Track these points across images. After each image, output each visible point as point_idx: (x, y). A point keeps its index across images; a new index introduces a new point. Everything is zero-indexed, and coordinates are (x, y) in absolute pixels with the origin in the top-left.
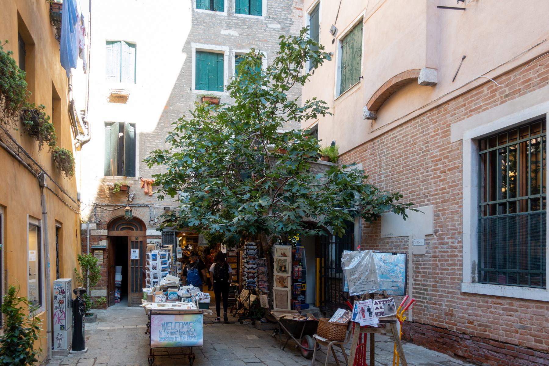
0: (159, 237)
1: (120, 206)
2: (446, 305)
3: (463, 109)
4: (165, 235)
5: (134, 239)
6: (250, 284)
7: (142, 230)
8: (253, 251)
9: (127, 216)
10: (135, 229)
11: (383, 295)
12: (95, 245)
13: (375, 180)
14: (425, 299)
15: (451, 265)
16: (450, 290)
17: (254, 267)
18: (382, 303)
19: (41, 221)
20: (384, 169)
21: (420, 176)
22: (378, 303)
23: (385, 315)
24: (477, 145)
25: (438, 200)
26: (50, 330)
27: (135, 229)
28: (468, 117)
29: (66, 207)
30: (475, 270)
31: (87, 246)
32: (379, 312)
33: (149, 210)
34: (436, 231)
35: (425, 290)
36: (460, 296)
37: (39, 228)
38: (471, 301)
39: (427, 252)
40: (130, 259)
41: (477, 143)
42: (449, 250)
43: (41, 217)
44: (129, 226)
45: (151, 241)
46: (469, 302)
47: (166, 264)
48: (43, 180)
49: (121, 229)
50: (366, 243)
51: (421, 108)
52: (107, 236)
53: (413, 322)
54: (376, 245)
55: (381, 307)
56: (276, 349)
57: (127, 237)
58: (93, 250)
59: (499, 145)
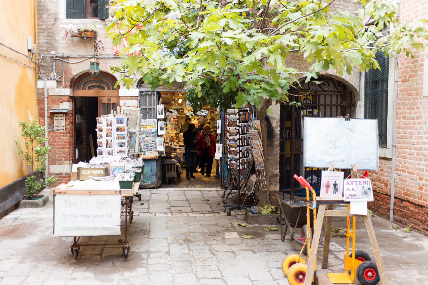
1: (88, 57)
4: (143, 96)
5: (105, 100)
6: (232, 162)
9: (93, 70)
10: (106, 88)
11: (158, 136)
12: (56, 108)
13: (417, 11)
17: (236, 139)
18: (354, 183)
22: (350, 183)
23: (357, 198)
27: (106, 88)
31: (44, 109)
32: (350, 195)
40: (303, 166)
44: (98, 84)
45: (125, 104)
49: (89, 87)
50: (403, 104)
52: (69, 96)
54: (415, 107)
55: (353, 189)
56: (257, 255)
57: (96, 98)
58: (52, 114)
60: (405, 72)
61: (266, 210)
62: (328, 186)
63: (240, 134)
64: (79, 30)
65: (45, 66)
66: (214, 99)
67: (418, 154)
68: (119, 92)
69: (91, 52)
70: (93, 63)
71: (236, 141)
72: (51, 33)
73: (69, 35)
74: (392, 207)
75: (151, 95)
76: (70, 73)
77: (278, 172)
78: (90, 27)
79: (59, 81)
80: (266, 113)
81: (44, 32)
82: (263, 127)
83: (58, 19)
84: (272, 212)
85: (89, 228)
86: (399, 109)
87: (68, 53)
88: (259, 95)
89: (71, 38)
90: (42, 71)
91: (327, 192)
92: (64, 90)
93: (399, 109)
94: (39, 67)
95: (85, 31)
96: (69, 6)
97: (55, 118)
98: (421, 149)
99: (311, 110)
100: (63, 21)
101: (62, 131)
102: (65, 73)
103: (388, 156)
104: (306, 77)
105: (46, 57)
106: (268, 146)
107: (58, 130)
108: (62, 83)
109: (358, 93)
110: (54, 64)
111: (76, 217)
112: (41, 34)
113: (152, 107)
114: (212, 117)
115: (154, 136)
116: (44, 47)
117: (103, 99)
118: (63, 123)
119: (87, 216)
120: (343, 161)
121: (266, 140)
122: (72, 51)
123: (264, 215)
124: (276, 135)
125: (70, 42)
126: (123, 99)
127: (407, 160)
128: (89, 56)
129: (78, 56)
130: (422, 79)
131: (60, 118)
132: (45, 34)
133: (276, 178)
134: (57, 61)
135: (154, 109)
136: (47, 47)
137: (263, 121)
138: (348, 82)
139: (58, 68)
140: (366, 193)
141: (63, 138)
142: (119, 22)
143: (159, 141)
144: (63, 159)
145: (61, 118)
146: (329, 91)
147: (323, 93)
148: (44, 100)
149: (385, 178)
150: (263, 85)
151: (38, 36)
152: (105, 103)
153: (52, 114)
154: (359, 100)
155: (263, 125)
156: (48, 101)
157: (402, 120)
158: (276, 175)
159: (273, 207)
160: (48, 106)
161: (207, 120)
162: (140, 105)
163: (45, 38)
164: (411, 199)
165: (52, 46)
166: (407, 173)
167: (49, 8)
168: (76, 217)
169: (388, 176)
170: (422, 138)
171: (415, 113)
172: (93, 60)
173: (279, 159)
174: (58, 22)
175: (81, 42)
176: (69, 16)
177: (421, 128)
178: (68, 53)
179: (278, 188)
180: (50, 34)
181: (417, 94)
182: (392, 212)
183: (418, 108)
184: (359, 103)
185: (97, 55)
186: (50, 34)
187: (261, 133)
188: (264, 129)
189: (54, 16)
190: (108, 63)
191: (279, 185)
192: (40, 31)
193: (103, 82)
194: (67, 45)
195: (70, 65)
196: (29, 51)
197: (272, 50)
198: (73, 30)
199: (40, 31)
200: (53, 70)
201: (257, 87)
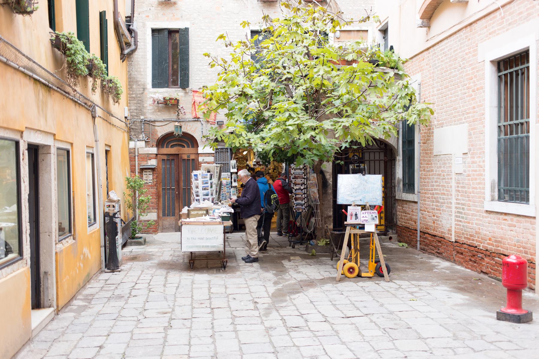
0: (213, 155)
2: (476, 224)
3: (485, 30)
4: (219, 152)
5: (185, 157)
7: (194, 147)
8: (299, 171)
13: (430, 92)
14: (463, 218)
15: (479, 184)
16: (479, 209)
18: (367, 213)
19: (95, 148)
20: (436, 82)
21: (460, 92)
24: (497, 66)
25: (471, 119)
26: (103, 244)
27: (186, 146)
28: (488, 39)
29: (114, 129)
30: (494, 188)
31: (135, 166)
33: (200, 125)
34: (470, 150)
35: (463, 209)
36: (485, 214)
37: (93, 155)
38: (491, 218)
39: (465, 171)
41: (496, 64)
42: (478, 169)
43: (94, 145)
44: (179, 143)
46: (489, 219)
47: (207, 183)
48: (95, 112)
49: (171, 146)
51: (459, 24)
53: (456, 242)
54: (430, 162)
56: (313, 266)
58: (142, 170)
59: (521, 65)
60: (424, 136)
61: (322, 243)
62: (352, 215)
63: (305, 185)
64: (164, 98)
65: (135, 129)
66: (280, 157)
67: (432, 198)
68: (198, 149)
69: (174, 116)
70: (178, 126)
71: (302, 190)
72: (140, 100)
73: (156, 102)
74: (418, 239)
75: (225, 152)
76: (156, 134)
77: (331, 213)
78: (174, 96)
79: (147, 142)
80: (320, 168)
81: (134, 100)
82: (319, 179)
83: (146, 88)
84: (326, 244)
85: (203, 246)
86: (421, 164)
87: (155, 117)
88: (312, 158)
89: (157, 105)
90: (133, 133)
91: (351, 219)
92: (151, 149)
93: (421, 164)
94: (130, 130)
95: (171, 99)
96: (154, 77)
97: (144, 173)
98: (433, 194)
99: (358, 164)
100: (150, 90)
101: (150, 184)
102: (152, 135)
103: (416, 200)
104: (342, 146)
105: (136, 121)
106: (323, 193)
107: (147, 183)
108: (149, 143)
109: (397, 151)
110: (143, 127)
111: (195, 239)
112: (132, 102)
113: (226, 162)
114: (275, 166)
115: (228, 187)
116: (134, 112)
117: (183, 155)
118: (151, 177)
119: (202, 239)
120: (361, 200)
121: (321, 189)
122: (158, 115)
123: (320, 246)
124: (329, 185)
125: (156, 108)
126: (201, 156)
127: (427, 202)
128: (172, 120)
129: (163, 120)
130: (433, 143)
131: (148, 173)
132: (135, 102)
133: (330, 219)
134: (145, 124)
135: (228, 163)
136: (137, 113)
137: (318, 174)
138: (388, 142)
139: (146, 130)
140: (373, 219)
141: (151, 190)
142: (209, 102)
143: (233, 192)
144: (151, 208)
145: (150, 173)
146: (373, 149)
147: (368, 151)
148: (135, 158)
149: (415, 217)
150: (315, 152)
151: (129, 103)
152: (185, 159)
153: (142, 170)
154: (398, 156)
155: (318, 177)
156: (138, 158)
157: (423, 172)
158: (330, 217)
159: (327, 240)
160: (138, 163)
161: (270, 169)
162: (216, 161)
163: (135, 105)
164: (429, 231)
165: (141, 111)
166: (426, 213)
167: (138, 79)
168: (195, 239)
169: (416, 216)
170: (433, 186)
171: (430, 167)
172: (177, 124)
173: (332, 204)
174: (146, 91)
175: (166, 107)
176: (154, 86)
177: (433, 178)
178: (155, 117)
179: (331, 226)
180: (139, 102)
181: (431, 153)
182: (419, 243)
183: (431, 164)
184: (398, 158)
185: (179, 119)
186: (139, 102)
187: (519, 158)
188: (319, 181)
189: (142, 86)
190: (189, 125)
191: (332, 224)
192: (131, 99)
193: (184, 142)
194: (154, 110)
195: (156, 128)
196: (126, 118)
197: (318, 133)
198: (160, 98)
199: (131, 99)
200: (142, 132)
201: (310, 153)
